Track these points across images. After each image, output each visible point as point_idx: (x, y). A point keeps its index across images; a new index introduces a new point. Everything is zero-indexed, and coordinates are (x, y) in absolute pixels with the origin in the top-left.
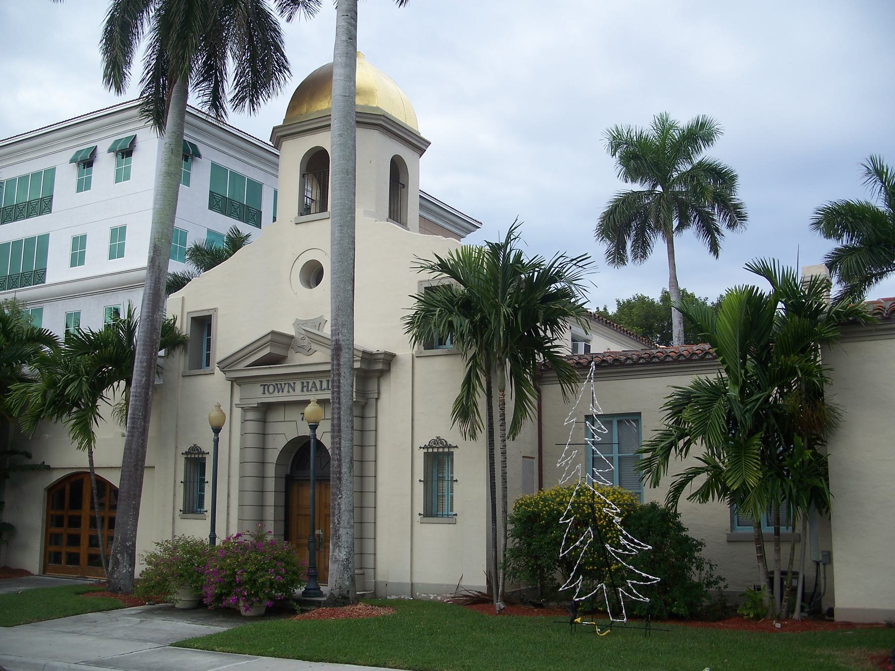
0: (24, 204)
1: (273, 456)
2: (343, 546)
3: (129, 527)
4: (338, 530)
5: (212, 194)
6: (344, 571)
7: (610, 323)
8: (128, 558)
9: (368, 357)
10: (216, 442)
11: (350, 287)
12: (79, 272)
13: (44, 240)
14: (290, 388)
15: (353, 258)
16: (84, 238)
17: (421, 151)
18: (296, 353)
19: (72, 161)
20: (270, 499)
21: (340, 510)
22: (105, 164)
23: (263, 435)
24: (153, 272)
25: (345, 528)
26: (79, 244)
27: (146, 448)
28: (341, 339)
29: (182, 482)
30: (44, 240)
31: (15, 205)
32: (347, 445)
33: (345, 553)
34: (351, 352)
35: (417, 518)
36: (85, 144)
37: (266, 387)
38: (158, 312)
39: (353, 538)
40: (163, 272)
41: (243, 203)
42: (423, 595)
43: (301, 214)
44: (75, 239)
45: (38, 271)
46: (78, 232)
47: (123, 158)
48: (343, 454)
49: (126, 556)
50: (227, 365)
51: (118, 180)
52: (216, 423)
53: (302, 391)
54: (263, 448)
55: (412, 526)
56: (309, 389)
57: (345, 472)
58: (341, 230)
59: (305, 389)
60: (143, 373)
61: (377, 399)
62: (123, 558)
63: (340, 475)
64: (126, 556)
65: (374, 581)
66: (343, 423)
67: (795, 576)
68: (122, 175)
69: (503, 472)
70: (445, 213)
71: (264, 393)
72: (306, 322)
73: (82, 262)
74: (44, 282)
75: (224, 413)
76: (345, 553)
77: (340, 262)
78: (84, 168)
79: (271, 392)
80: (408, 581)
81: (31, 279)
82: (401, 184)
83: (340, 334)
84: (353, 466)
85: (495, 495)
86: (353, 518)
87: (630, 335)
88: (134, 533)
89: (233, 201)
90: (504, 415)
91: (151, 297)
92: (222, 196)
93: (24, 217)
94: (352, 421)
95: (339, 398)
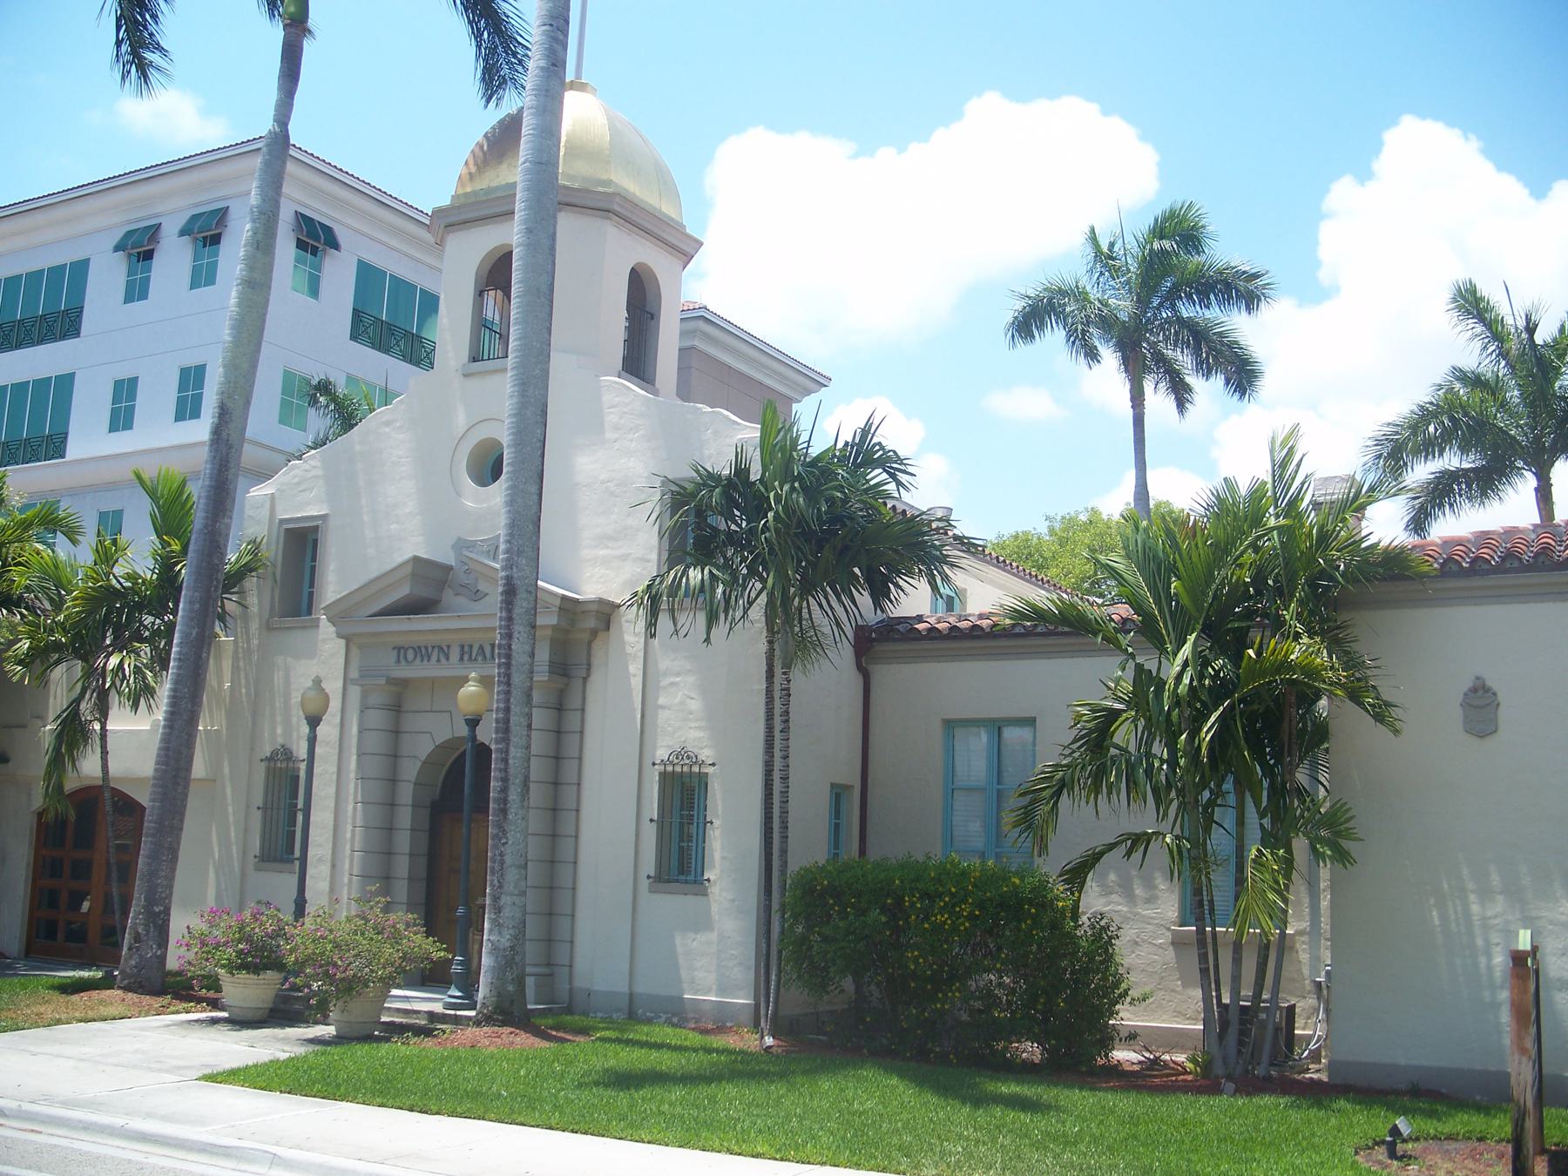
0: (56, 314)
1: (410, 770)
2: (505, 925)
3: (159, 881)
4: (499, 898)
5: (357, 315)
6: (506, 967)
7: (1004, 561)
8: (156, 933)
9: (570, 608)
10: (312, 741)
11: (534, 489)
12: (123, 442)
13: (65, 383)
14: (441, 655)
15: (542, 439)
16: (133, 382)
17: (687, 257)
18: (456, 595)
19: (117, 248)
20: (403, 842)
21: (503, 864)
22: (174, 258)
23: (396, 732)
24: (216, 451)
25: (512, 895)
26: (125, 391)
27: (160, 749)
28: (516, 576)
29: (259, 808)
30: (65, 383)
31: (19, 321)
32: (519, 755)
33: (508, 937)
34: (532, 599)
35: (645, 884)
36: (138, 218)
37: (402, 651)
38: (223, 518)
39: (524, 913)
40: (234, 450)
41: (411, 331)
42: (648, 1014)
43: (474, 358)
44: (118, 384)
45: (54, 437)
46: (124, 373)
47: (204, 246)
48: (511, 771)
49: (152, 929)
50: (341, 615)
51: (194, 284)
52: (312, 708)
53: (462, 659)
54: (394, 756)
55: (635, 898)
56: (473, 658)
57: (513, 800)
58: (523, 391)
59: (466, 657)
60: (192, 621)
61: (585, 679)
62: (148, 932)
63: (505, 804)
64: (152, 929)
65: (568, 987)
66: (513, 719)
67: (114, 875)
68: (203, 276)
69: (783, 810)
70: (764, 359)
71: (398, 661)
72: (472, 545)
73: (128, 425)
74: (62, 456)
75: (326, 693)
76: (508, 937)
77: (519, 445)
78: (138, 261)
79: (410, 660)
80: (626, 990)
81: (42, 449)
82: (648, 313)
83: (514, 568)
84: (528, 790)
85: (772, 848)
86: (526, 878)
87: (1043, 584)
88: (168, 892)
89: (393, 328)
90: (788, 713)
91: (212, 493)
92: (375, 318)
93: (56, 338)
94: (530, 716)
95: (508, 676)
